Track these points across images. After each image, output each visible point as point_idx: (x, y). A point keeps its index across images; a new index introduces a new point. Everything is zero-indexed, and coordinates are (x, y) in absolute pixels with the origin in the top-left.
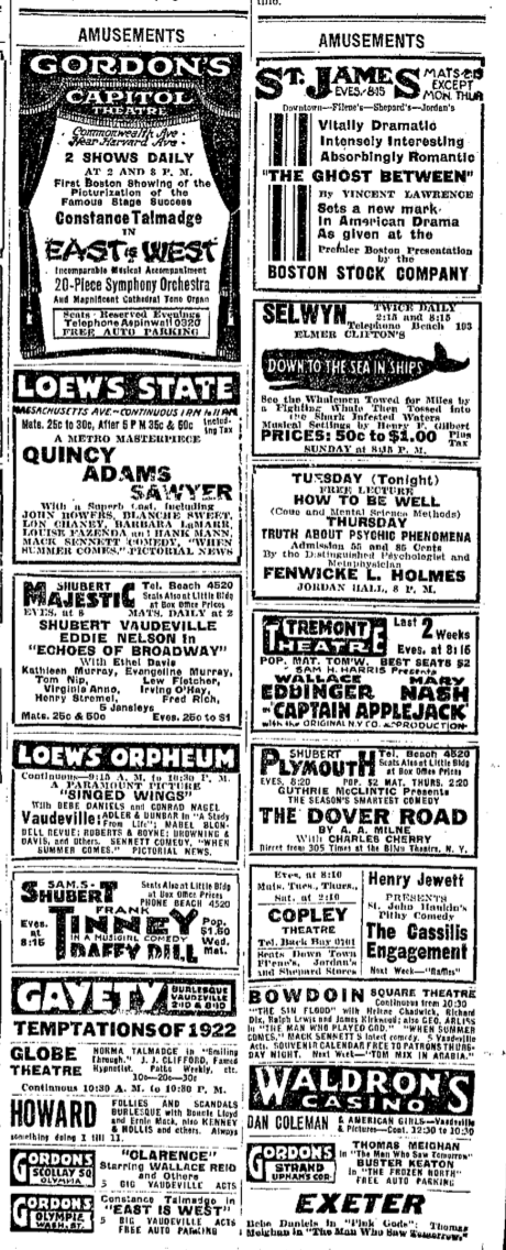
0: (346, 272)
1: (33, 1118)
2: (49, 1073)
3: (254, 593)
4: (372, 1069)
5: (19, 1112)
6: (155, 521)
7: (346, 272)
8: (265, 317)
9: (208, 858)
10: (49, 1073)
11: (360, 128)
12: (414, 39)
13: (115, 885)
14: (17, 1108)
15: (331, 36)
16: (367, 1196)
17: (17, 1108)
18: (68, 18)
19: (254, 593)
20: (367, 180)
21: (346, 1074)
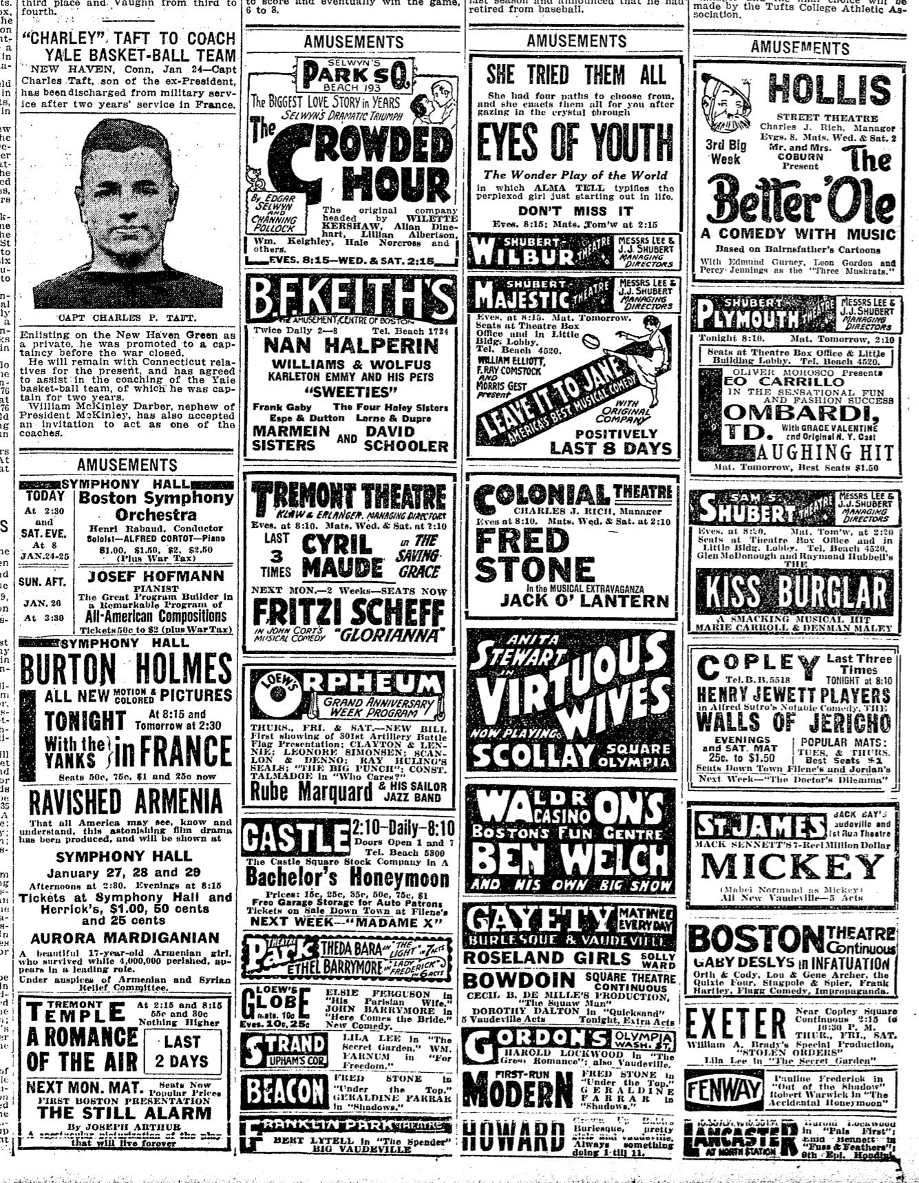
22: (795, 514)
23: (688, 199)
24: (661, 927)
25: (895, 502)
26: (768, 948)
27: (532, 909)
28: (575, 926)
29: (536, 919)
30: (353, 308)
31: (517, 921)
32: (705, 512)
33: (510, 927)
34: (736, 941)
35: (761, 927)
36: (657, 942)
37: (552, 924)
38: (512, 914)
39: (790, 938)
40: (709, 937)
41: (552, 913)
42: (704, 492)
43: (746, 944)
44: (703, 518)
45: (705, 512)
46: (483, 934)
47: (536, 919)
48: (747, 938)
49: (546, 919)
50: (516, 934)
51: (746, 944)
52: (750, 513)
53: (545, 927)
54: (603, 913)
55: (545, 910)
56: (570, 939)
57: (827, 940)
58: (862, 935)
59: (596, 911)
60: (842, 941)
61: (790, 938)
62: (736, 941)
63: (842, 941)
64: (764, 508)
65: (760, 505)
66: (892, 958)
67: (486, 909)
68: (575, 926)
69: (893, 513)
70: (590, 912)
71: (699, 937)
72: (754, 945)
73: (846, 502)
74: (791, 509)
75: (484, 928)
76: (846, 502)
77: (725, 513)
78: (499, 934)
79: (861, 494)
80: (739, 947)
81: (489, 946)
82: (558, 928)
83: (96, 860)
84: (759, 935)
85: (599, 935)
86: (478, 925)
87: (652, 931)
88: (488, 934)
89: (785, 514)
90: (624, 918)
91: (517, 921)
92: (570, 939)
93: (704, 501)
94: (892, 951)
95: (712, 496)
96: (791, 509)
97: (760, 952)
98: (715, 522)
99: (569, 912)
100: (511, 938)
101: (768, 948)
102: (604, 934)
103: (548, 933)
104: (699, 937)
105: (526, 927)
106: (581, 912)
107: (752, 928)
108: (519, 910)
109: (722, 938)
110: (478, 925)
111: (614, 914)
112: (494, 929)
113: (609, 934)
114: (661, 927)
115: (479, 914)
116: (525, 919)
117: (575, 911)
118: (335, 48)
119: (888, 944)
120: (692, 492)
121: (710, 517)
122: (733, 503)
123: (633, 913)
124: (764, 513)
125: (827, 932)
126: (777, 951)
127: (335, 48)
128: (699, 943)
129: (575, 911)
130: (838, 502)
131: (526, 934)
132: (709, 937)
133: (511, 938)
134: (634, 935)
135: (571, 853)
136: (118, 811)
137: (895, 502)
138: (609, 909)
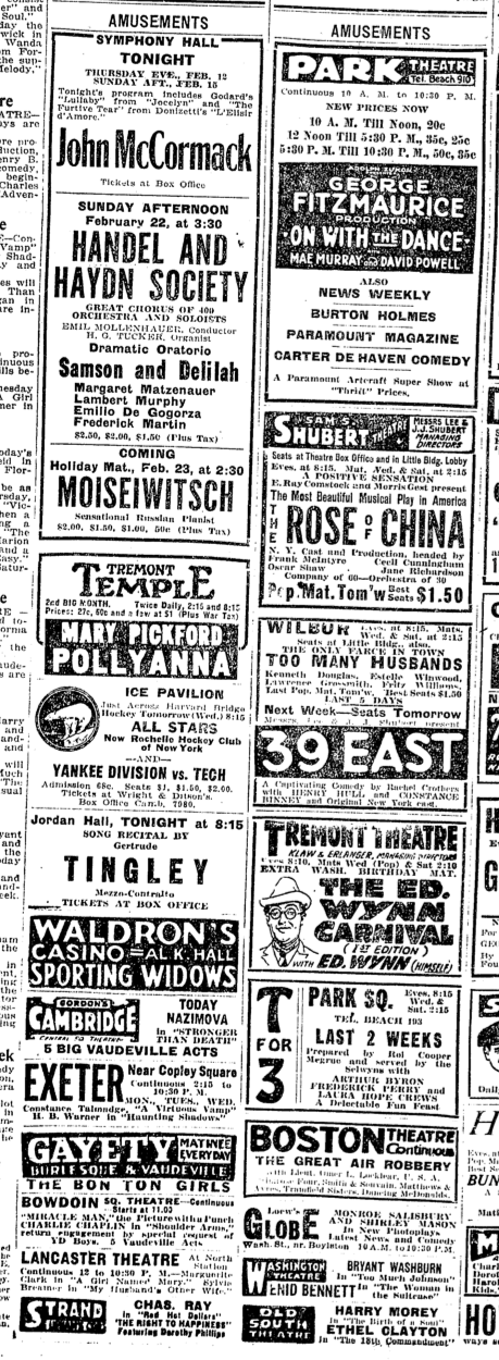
0: (80, 1258)
1: (133, 254)
2: (122, 210)
3: (266, 395)
4: (112, 919)
5: (476, 1319)
6: (43, 1222)
7: (80, 1258)
8: (191, 503)
9: (217, 445)
10: (122, 210)
11: (182, 404)
12: (199, 21)
13: (64, 361)
14: (473, 1314)
15: (42, 1254)
16: (77, 1066)
17: (473, 1314)
18: (318, 15)
19: (266, 395)
20: (189, 63)
21: (111, 926)
22: (368, 439)
23: (266, 117)
24: (221, 1156)
25: (469, 428)
26: (329, 1148)
27: (92, 1140)
28: (134, 1157)
29: (95, 1152)
30: (348, 209)
31: (77, 1152)
32: (279, 434)
33: (70, 1158)
34: (299, 1141)
35: (322, 1129)
36: (217, 1171)
37: (112, 1155)
38: (73, 1146)
39: (350, 1140)
40: (271, 1137)
41: (112, 1144)
42: (278, 414)
43: (307, 1144)
44: (278, 439)
45: (279, 434)
46: (44, 1165)
47: (95, 1152)
48: (310, 1140)
49: (106, 1150)
50: (77, 1165)
51: (307, 1144)
52: (324, 436)
53: (105, 1158)
54: (163, 1143)
55: (105, 1141)
56: (130, 1169)
57: (387, 1141)
58: (421, 1137)
59: (156, 1141)
60: (402, 1143)
61: (350, 1140)
62: (299, 1141)
63: (402, 1143)
64: (338, 431)
65: (333, 428)
66: (451, 1160)
67: (46, 1141)
68: (134, 1157)
69: (466, 438)
70: (150, 1143)
71: (261, 1137)
72: (315, 1146)
73: (420, 427)
74: (364, 433)
75: (45, 1159)
76: (420, 427)
77: (300, 435)
78: (60, 1164)
79: (437, 420)
80: (301, 1148)
81: (49, 1176)
82: (118, 1158)
83: (114, 425)
84: (320, 1137)
85: (159, 1165)
86: (39, 1156)
87: (211, 1161)
88: (49, 1165)
89: (359, 438)
90: (184, 1147)
91: (77, 1152)
92: (130, 1169)
93: (279, 423)
94: (450, 1153)
95: (287, 418)
96: (364, 433)
97: (321, 1153)
98: (290, 444)
99: (128, 1142)
100: (72, 1169)
101: (329, 1148)
102: (165, 1164)
103: (108, 1164)
104: (261, 1137)
105: (86, 1158)
106: (140, 1143)
107: (314, 1130)
108: (79, 1141)
109: (284, 1139)
110: (39, 1156)
111: (174, 1143)
112: (55, 1160)
113: (170, 1163)
114: (221, 1156)
115: (41, 1145)
116: (86, 1150)
117: (134, 1141)
118: (139, 28)
119: (446, 1146)
120: (267, 414)
121: (285, 438)
122: (306, 426)
123: (194, 1143)
124: (338, 436)
125: (387, 1134)
126: (337, 1150)
127: (139, 28)
128: (260, 1142)
129: (134, 1141)
130: (412, 426)
131: (87, 1165)
132: (271, 1137)
133: (72, 1169)
134: (195, 1165)
135: (149, 972)
136: (223, 262)
137: (469, 428)
138: (169, 1140)
